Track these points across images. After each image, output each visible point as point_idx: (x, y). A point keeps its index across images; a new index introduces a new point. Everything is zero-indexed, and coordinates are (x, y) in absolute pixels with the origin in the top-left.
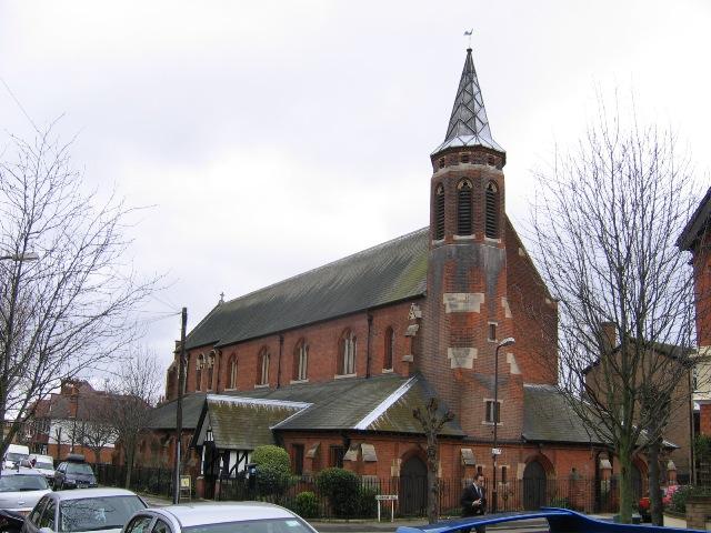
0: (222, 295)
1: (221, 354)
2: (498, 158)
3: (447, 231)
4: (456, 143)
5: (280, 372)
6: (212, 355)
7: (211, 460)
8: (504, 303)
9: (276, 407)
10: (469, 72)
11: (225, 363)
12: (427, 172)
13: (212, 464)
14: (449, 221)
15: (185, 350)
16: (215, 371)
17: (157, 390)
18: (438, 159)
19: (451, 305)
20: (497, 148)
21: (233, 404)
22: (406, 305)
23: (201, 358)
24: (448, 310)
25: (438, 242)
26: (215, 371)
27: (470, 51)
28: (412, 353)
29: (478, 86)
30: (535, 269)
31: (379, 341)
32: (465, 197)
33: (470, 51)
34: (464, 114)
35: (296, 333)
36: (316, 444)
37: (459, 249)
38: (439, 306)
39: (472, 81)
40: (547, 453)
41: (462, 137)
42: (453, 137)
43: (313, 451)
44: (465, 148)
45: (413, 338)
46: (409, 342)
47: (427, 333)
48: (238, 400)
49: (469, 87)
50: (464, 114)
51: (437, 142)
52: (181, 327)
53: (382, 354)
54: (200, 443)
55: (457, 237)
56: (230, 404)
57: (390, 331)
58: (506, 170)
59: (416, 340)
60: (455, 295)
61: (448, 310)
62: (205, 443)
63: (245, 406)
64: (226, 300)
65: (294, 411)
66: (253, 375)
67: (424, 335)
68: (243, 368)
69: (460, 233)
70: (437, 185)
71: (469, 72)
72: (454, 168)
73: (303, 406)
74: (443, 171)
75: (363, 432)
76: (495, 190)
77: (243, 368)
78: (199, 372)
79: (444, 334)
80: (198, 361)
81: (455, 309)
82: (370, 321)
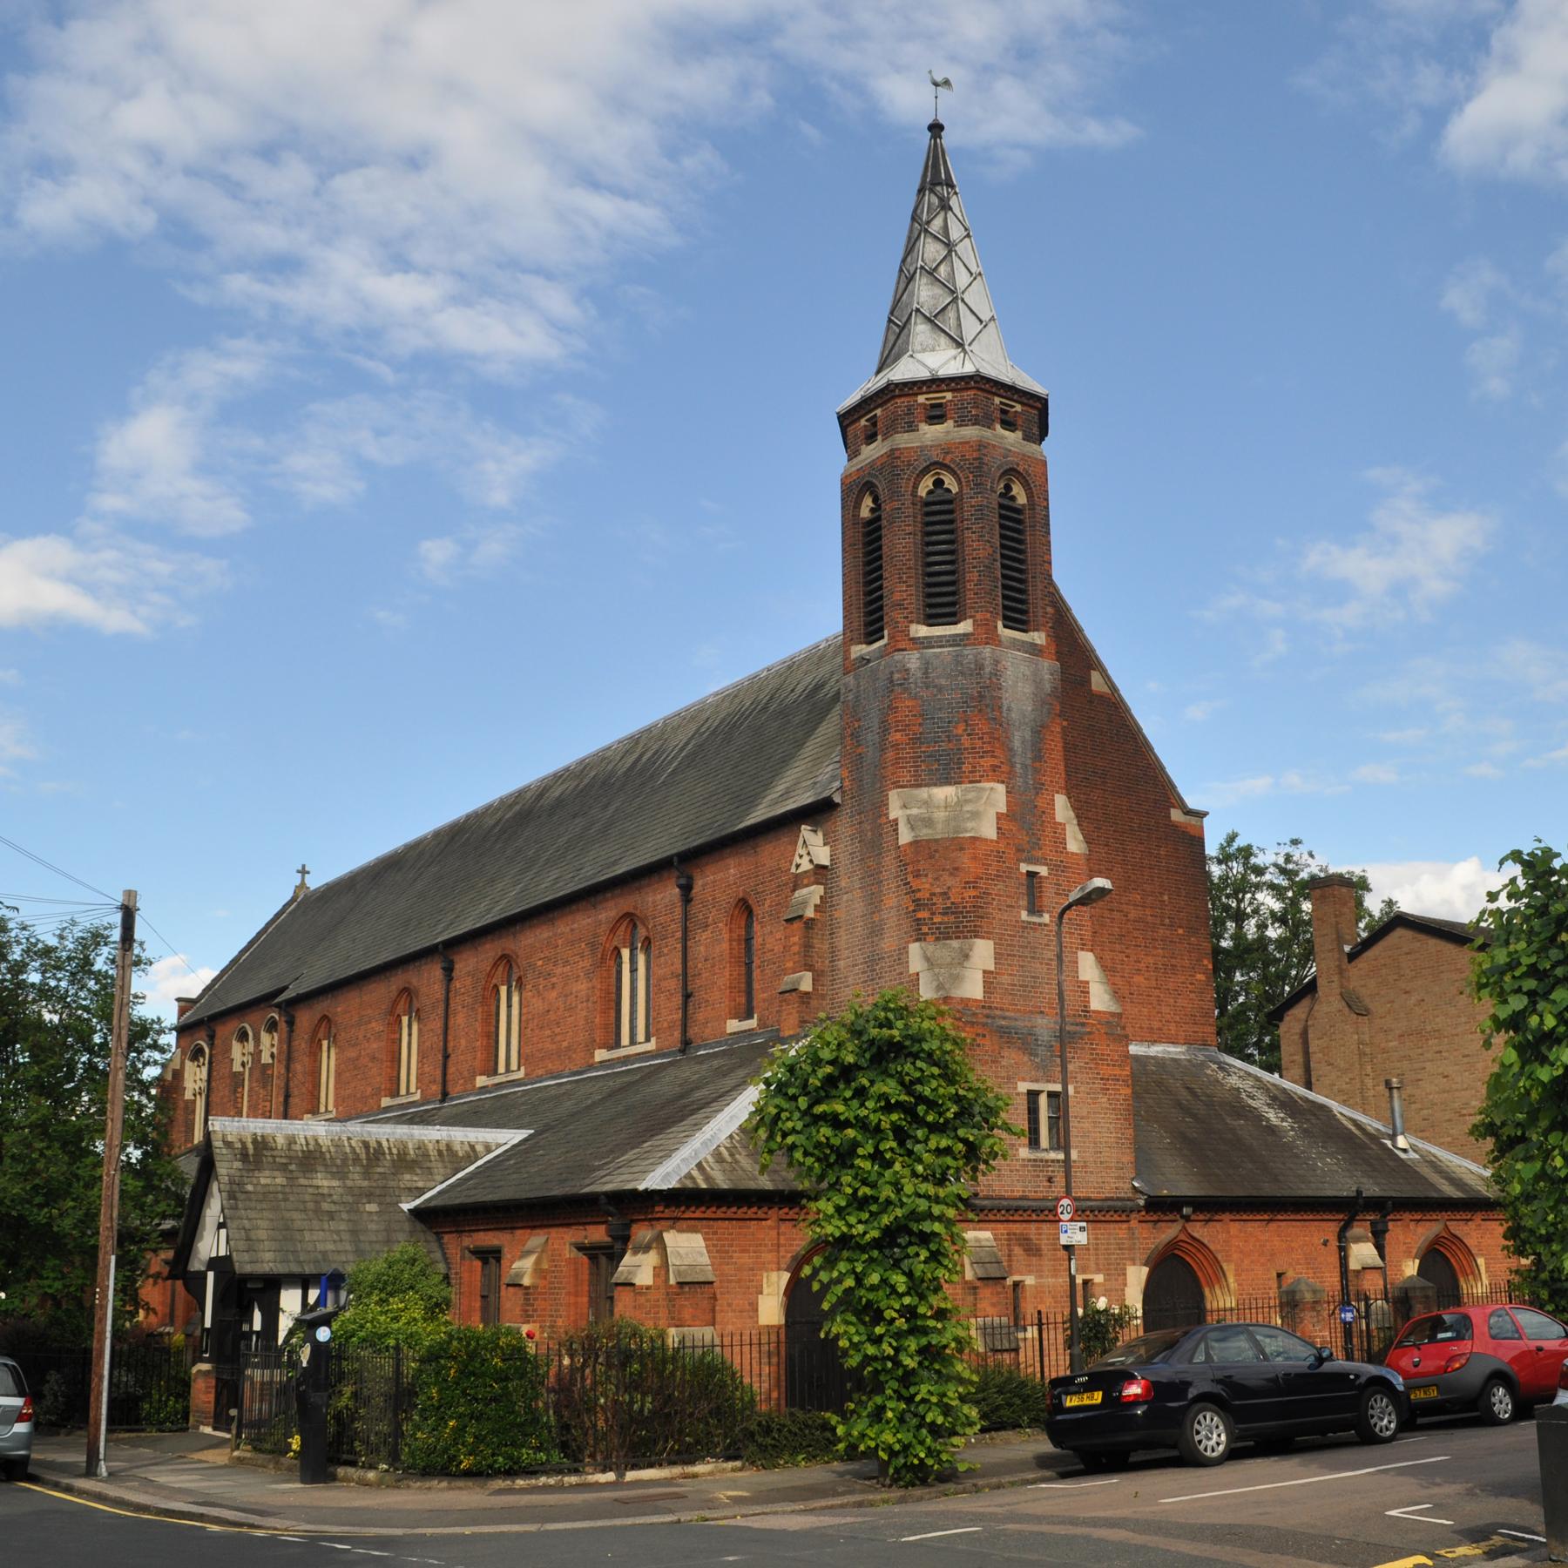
1: (291, 1023)
3: (892, 615)
4: (904, 370)
5: (446, 1057)
6: (272, 1027)
8: (1062, 809)
12: (830, 462)
14: (902, 589)
21: (291, 1140)
24: (905, 837)
38: (877, 830)
54: (196, 1265)
55: (921, 631)
61: (905, 837)
62: (214, 1263)
64: (315, 882)
67: (841, 914)
68: (352, 1053)
69: (931, 620)
70: (855, 489)
73: (511, 1137)
77: (352, 1053)
81: (925, 833)
82: (686, 889)
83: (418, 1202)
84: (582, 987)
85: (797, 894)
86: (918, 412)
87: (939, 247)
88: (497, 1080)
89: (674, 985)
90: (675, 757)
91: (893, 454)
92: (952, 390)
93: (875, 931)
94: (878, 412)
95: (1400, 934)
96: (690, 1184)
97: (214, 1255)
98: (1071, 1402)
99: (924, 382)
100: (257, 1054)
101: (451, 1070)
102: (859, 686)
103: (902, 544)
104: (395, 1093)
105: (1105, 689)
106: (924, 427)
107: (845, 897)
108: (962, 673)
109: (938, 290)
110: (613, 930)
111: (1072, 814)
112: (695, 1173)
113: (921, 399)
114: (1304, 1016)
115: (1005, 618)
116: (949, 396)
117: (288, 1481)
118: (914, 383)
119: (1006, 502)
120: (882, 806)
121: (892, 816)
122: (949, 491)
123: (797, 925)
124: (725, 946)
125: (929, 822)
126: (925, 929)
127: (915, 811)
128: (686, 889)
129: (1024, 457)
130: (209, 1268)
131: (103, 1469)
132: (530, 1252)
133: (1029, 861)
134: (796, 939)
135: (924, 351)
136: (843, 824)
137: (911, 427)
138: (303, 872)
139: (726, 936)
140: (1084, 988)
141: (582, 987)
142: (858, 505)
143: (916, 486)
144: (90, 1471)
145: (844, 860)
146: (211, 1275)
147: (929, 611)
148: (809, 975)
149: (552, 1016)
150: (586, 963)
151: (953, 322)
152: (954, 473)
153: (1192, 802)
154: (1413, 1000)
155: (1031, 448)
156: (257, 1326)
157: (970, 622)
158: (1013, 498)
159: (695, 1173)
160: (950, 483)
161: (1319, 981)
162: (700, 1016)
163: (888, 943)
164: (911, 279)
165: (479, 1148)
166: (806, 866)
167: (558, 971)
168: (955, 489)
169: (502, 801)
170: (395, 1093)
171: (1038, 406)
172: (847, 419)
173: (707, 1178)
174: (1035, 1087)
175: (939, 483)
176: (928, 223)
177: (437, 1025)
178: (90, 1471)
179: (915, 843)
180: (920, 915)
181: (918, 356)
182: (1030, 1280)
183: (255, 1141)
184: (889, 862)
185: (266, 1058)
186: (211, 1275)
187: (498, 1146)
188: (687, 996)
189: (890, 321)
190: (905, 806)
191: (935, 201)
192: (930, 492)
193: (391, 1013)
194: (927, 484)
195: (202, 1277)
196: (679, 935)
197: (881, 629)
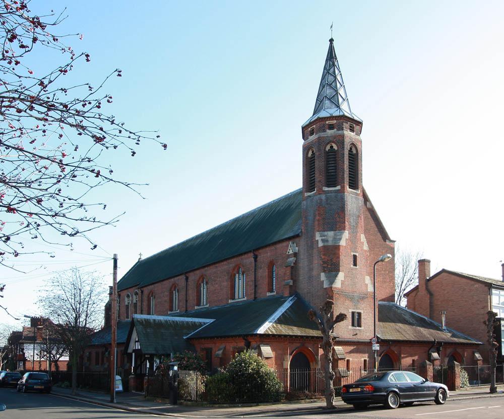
0: (140, 255)
1: (142, 292)
2: (355, 124)
3: (317, 184)
4: (323, 114)
5: (186, 301)
6: (136, 294)
7: (139, 363)
8: (363, 238)
9: (187, 322)
10: (331, 56)
11: (145, 298)
12: (299, 143)
13: (140, 365)
14: (319, 177)
15: (120, 289)
16: (139, 304)
17: (97, 322)
18: (307, 130)
19: (323, 241)
20: (356, 118)
21: (154, 320)
22: (284, 244)
23: (128, 296)
24: (320, 244)
25: (310, 194)
26: (139, 304)
27: (331, 41)
28: (292, 279)
29: (339, 70)
30: (235, 289)
31: (263, 273)
32: (332, 158)
33: (331, 41)
34: (328, 92)
35: (197, 272)
36: (222, 346)
37: (327, 199)
38: (312, 243)
39: (334, 65)
40: (395, 349)
41: (328, 110)
42: (320, 111)
43: (221, 352)
44: (332, 118)
45: (292, 267)
46: (288, 271)
47: (303, 264)
48: (161, 318)
49: (332, 70)
50: (328, 92)
51: (306, 114)
52: (112, 271)
53: (266, 281)
54: (130, 351)
55: (326, 189)
56: (152, 321)
57: (271, 265)
58: (363, 136)
59: (294, 270)
60: (326, 233)
61: (320, 244)
62: (135, 351)
63: (163, 322)
64: (144, 258)
65: (205, 324)
66: (167, 305)
67: (301, 265)
68: (159, 300)
69: (328, 186)
70: (306, 149)
71: (331, 56)
72: (322, 134)
73: (209, 321)
74: (312, 138)
75: (260, 335)
76: (354, 152)
77: (159, 300)
78: (127, 307)
79: (317, 262)
80: (126, 299)
81: (326, 244)
82: (256, 258)
83: (188, 336)
84: (225, 284)
85: (288, 260)
86: (327, 126)
87: (332, 77)
88: (201, 307)
89: (252, 284)
90: (248, 224)
91: (319, 138)
92: (336, 120)
93: (311, 270)
94: (314, 126)
95: (443, 274)
96: (267, 333)
97: (134, 348)
98: (351, 390)
99: (328, 118)
100: (132, 300)
101: (188, 304)
102: (307, 204)
103: (319, 164)
104: (233, 298)
105: (370, 207)
106: (328, 131)
107: (302, 261)
108: (337, 200)
109: (332, 91)
110: (234, 269)
111: (365, 240)
112: (268, 330)
113: (327, 122)
114: (414, 296)
115: (349, 185)
116: (335, 121)
117: (165, 404)
118: (325, 118)
119: (350, 153)
120: (313, 236)
121: (316, 239)
122: (334, 149)
123: (289, 268)
124: (267, 273)
125: (327, 241)
126: (326, 269)
127: (323, 238)
128: (256, 258)
129: (355, 139)
130: (133, 352)
131: (115, 401)
132: (221, 349)
133: (353, 252)
134: (288, 271)
135: (328, 109)
136: (302, 241)
137: (324, 131)
138: (140, 255)
139: (267, 271)
140: (367, 285)
141: (225, 284)
142: (307, 153)
143: (325, 148)
144: (112, 401)
145: (302, 251)
146: (134, 354)
147: (328, 183)
148: (292, 281)
149: (216, 291)
150: (226, 278)
151: (336, 100)
152: (336, 144)
153: (392, 238)
154: (446, 292)
155: (357, 137)
156: (148, 366)
157: (340, 186)
158: (352, 152)
159: (268, 330)
160: (335, 147)
161: (419, 287)
162: (259, 291)
163: (315, 273)
164: (324, 87)
165: (202, 323)
166: (291, 252)
167: (218, 280)
168: (336, 148)
169: (207, 231)
170: (233, 298)
171: (359, 123)
172: (304, 129)
173: (271, 331)
174: (354, 311)
175: (332, 147)
176: (329, 70)
177: (183, 292)
178: (112, 401)
179: (324, 247)
180: (324, 265)
181: (327, 110)
182: (351, 359)
183: (145, 320)
184: (315, 251)
185: (238, 275)
186: (134, 354)
187: (207, 323)
188: (256, 286)
189: (317, 100)
190: (321, 236)
191: (331, 63)
192: (329, 150)
193: (170, 290)
194: (328, 148)
195: (131, 354)
196: (253, 270)
197: (314, 188)
